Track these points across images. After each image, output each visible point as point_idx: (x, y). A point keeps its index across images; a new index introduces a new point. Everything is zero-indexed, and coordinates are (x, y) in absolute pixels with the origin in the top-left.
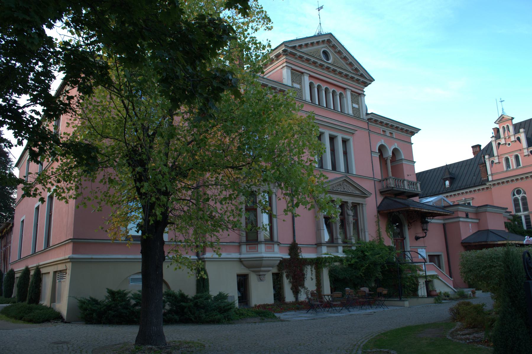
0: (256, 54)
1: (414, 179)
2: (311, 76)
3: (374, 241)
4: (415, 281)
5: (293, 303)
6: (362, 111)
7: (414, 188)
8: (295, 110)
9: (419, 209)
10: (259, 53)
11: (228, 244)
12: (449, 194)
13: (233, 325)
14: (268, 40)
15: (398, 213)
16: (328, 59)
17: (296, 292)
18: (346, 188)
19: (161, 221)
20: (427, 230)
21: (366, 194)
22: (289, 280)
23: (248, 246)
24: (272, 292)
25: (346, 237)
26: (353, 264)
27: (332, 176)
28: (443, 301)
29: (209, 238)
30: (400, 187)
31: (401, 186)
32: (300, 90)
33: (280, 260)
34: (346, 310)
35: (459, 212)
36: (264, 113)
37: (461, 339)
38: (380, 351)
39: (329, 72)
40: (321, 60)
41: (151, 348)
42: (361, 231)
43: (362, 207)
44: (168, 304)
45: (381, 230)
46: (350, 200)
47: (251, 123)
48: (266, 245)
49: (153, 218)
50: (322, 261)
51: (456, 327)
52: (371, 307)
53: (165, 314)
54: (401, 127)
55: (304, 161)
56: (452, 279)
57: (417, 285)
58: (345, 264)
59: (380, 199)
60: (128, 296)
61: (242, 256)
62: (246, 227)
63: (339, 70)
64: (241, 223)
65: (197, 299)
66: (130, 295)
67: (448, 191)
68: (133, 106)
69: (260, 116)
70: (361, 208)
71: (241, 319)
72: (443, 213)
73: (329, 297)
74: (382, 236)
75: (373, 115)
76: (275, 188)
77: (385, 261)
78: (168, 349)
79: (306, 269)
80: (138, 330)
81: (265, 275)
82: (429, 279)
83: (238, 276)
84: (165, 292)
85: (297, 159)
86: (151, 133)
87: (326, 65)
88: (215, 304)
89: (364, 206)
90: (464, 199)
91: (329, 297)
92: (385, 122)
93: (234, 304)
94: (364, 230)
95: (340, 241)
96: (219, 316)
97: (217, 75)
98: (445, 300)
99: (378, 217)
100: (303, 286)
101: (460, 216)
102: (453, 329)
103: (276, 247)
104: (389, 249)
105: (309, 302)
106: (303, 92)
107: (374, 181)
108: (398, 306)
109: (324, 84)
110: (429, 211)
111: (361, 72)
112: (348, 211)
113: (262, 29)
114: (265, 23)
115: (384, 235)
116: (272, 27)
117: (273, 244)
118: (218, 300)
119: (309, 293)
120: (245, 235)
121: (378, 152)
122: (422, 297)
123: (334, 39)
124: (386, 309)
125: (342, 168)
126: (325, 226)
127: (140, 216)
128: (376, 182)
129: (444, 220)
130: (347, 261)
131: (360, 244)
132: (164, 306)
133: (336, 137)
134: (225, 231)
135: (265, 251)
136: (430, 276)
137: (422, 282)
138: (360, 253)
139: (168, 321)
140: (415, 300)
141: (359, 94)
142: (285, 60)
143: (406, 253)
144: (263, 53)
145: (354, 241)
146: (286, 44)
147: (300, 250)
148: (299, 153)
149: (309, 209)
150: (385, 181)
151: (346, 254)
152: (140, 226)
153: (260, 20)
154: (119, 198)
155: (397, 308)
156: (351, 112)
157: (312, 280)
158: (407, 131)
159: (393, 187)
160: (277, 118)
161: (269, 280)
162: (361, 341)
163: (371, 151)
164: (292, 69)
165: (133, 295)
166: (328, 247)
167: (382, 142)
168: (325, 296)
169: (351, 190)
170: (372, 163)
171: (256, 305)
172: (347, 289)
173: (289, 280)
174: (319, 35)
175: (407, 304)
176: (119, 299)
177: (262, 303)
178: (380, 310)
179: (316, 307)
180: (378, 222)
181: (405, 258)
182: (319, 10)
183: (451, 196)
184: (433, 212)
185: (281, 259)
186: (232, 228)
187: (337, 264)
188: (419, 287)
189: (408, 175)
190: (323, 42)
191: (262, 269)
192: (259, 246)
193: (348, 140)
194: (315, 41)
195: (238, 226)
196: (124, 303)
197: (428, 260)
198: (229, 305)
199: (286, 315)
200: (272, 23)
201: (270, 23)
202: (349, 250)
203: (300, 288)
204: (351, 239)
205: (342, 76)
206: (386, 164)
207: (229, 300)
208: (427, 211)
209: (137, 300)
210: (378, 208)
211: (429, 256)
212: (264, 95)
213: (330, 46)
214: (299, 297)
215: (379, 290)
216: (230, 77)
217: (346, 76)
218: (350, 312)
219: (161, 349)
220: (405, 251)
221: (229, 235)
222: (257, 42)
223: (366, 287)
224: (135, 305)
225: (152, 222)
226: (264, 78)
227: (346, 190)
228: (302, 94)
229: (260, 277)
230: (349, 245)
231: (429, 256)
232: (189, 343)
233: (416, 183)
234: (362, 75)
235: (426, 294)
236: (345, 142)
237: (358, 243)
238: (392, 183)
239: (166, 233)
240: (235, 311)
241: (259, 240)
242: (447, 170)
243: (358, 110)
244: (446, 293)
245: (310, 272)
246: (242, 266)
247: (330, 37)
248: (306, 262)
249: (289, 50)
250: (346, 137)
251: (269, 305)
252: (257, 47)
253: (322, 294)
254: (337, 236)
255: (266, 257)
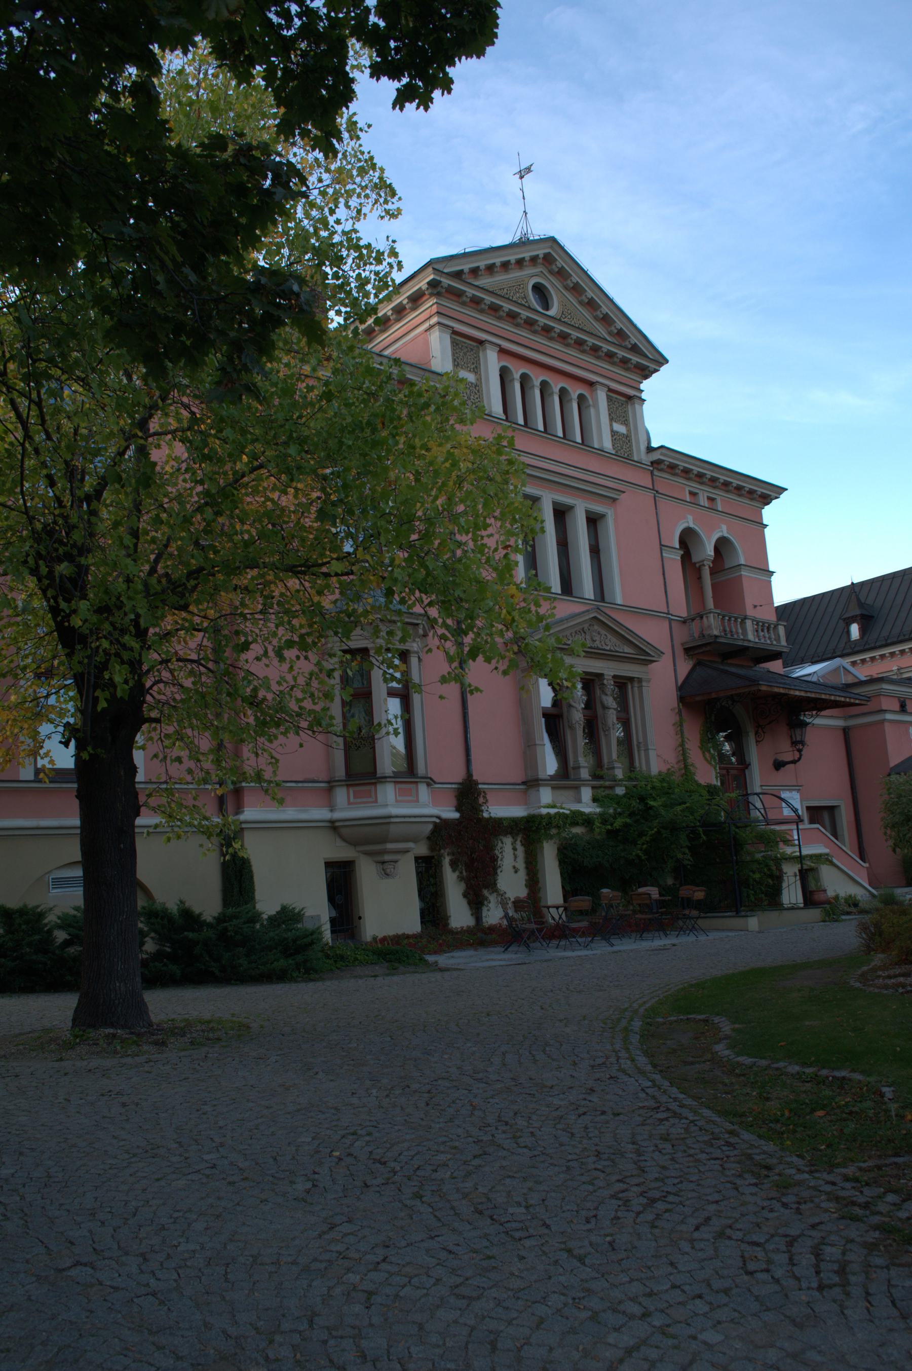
0: (360, 274)
1: (772, 618)
2: (502, 351)
3: (669, 773)
4: (774, 868)
5: (469, 931)
6: (638, 443)
7: (770, 638)
8: (462, 421)
9: (782, 691)
10: (367, 272)
11: (300, 785)
12: (857, 658)
13: (319, 984)
14: (390, 239)
15: (730, 702)
16: (546, 305)
17: (476, 903)
18: (597, 638)
19: (126, 698)
20: (802, 742)
21: (649, 655)
22: (457, 873)
23: (351, 790)
24: (415, 905)
25: (599, 763)
26: (618, 831)
27: (565, 609)
28: (844, 917)
29: (250, 762)
30: (735, 636)
31: (737, 633)
32: (477, 388)
33: (435, 823)
34: (604, 943)
35: (882, 697)
36: (383, 424)
37: (886, 987)
38: (688, 1019)
39: (551, 339)
40: (529, 308)
41: (114, 1035)
42: (638, 747)
43: (640, 687)
44: (152, 938)
45: (687, 746)
46: (608, 669)
47: (349, 447)
48: (398, 786)
49: (107, 694)
50: (540, 823)
51: (873, 964)
52: (666, 935)
53: (144, 964)
54: (735, 482)
55: (489, 548)
56: (866, 865)
57: (778, 878)
58: (597, 830)
59: (684, 667)
60: (46, 921)
61: (337, 815)
62: (345, 726)
63: (575, 334)
64: (332, 718)
65: (225, 921)
66: (51, 918)
67: (856, 649)
68: (42, 416)
69: (374, 431)
70: (636, 689)
71: (338, 969)
72: (843, 699)
73: (561, 910)
74: (689, 761)
75: (664, 451)
76: (417, 640)
77: (699, 821)
78: (157, 1034)
79: (500, 844)
80: (76, 1001)
81: (396, 862)
82: (808, 864)
83: (328, 865)
84: (144, 908)
85: (471, 544)
86: (89, 484)
87: (542, 321)
88: (271, 934)
89: (644, 684)
90: (895, 668)
91: (561, 910)
92: (696, 469)
93: (321, 933)
94: (646, 745)
95: (585, 774)
96: (282, 963)
97: (262, 282)
98: (848, 913)
99: (680, 713)
100: (492, 886)
101: (884, 708)
102: (865, 968)
103: (423, 791)
104: (709, 792)
105: (510, 925)
106: (484, 392)
107: (670, 620)
108: (731, 930)
109: (538, 370)
110: (809, 695)
111: (634, 340)
112: (604, 698)
113: (372, 214)
114: (382, 200)
115: (696, 756)
116: (399, 211)
117: (417, 782)
118: (279, 925)
119: (510, 905)
120: (342, 746)
121: (678, 546)
122: (792, 908)
123: (561, 252)
124: (702, 938)
125: (587, 588)
126: (546, 736)
127: (70, 706)
128: (674, 624)
129: (846, 718)
130: (604, 822)
131: (636, 779)
132: (142, 944)
133: (571, 508)
134: (291, 735)
135: (397, 801)
136: (811, 857)
137: (790, 871)
138: (635, 803)
139: (155, 980)
140: (773, 916)
141: (630, 398)
142: (435, 308)
143: (751, 799)
144: (377, 273)
145: (619, 774)
146: (436, 266)
147: (484, 797)
148: (477, 527)
149: (505, 673)
150: (698, 621)
151: (601, 806)
152: (71, 734)
153: (368, 191)
154: (12, 661)
155: (730, 934)
156: (608, 444)
157: (516, 872)
158: (751, 492)
159: (716, 637)
160: (417, 440)
161: (407, 871)
162: (640, 1002)
163: (661, 545)
164: (455, 332)
165: (59, 918)
166: (554, 788)
167: (690, 521)
168: (548, 907)
169: (611, 643)
170: (664, 574)
171: (375, 939)
172: (605, 891)
173: (457, 873)
174: (524, 242)
175: (753, 923)
176: (24, 927)
177: (391, 933)
178: (687, 939)
179: (529, 938)
180: (681, 725)
181: (748, 811)
182: (521, 177)
183: (863, 661)
184: (818, 696)
185: (438, 821)
186: (310, 728)
187: (578, 830)
188: (785, 885)
189: (755, 606)
190: (534, 259)
191: (390, 846)
192: (380, 787)
193: (602, 516)
194: (512, 258)
195: (324, 723)
196: (37, 937)
197: (806, 818)
198: (307, 936)
199: (453, 957)
200: (400, 199)
201: (393, 200)
202: (607, 796)
203: (486, 892)
204: (613, 768)
205: (583, 352)
206: (700, 578)
207: (309, 925)
208: (803, 694)
209: (71, 929)
210: (680, 689)
211: (808, 808)
212: (382, 382)
213: (551, 272)
214: (484, 915)
215: (685, 891)
216: (296, 288)
217: (595, 349)
218: (612, 945)
219: (139, 1035)
220: (747, 794)
221: (301, 745)
222: (362, 243)
223: (652, 885)
224: (67, 943)
225: (102, 705)
226: (381, 356)
227: (598, 644)
228: (480, 398)
229: (385, 868)
230: (607, 783)
231: (808, 808)
232: (209, 1022)
233: (776, 626)
234: (635, 349)
235: (800, 899)
236: (593, 521)
237: (630, 779)
238: (714, 626)
239: (140, 748)
240: (322, 951)
241: (379, 773)
242: (853, 596)
243: (627, 437)
244: (850, 896)
245: (512, 852)
246: (338, 840)
247: (551, 247)
248: (500, 827)
249: (446, 281)
250: (597, 508)
251: (408, 937)
252: (361, 257)
253: (542, 903)
254: (576, 761)
255: (397, 817)
